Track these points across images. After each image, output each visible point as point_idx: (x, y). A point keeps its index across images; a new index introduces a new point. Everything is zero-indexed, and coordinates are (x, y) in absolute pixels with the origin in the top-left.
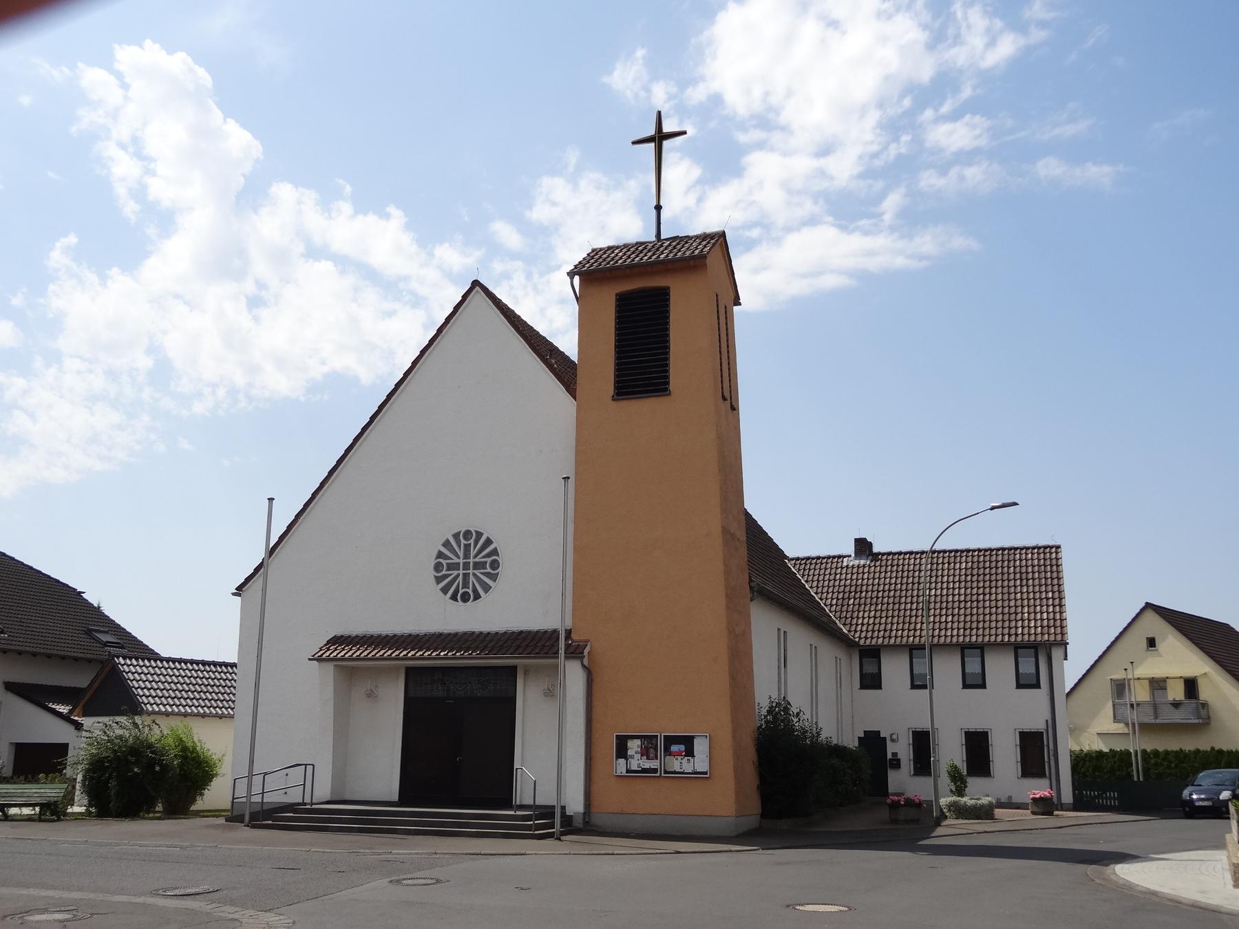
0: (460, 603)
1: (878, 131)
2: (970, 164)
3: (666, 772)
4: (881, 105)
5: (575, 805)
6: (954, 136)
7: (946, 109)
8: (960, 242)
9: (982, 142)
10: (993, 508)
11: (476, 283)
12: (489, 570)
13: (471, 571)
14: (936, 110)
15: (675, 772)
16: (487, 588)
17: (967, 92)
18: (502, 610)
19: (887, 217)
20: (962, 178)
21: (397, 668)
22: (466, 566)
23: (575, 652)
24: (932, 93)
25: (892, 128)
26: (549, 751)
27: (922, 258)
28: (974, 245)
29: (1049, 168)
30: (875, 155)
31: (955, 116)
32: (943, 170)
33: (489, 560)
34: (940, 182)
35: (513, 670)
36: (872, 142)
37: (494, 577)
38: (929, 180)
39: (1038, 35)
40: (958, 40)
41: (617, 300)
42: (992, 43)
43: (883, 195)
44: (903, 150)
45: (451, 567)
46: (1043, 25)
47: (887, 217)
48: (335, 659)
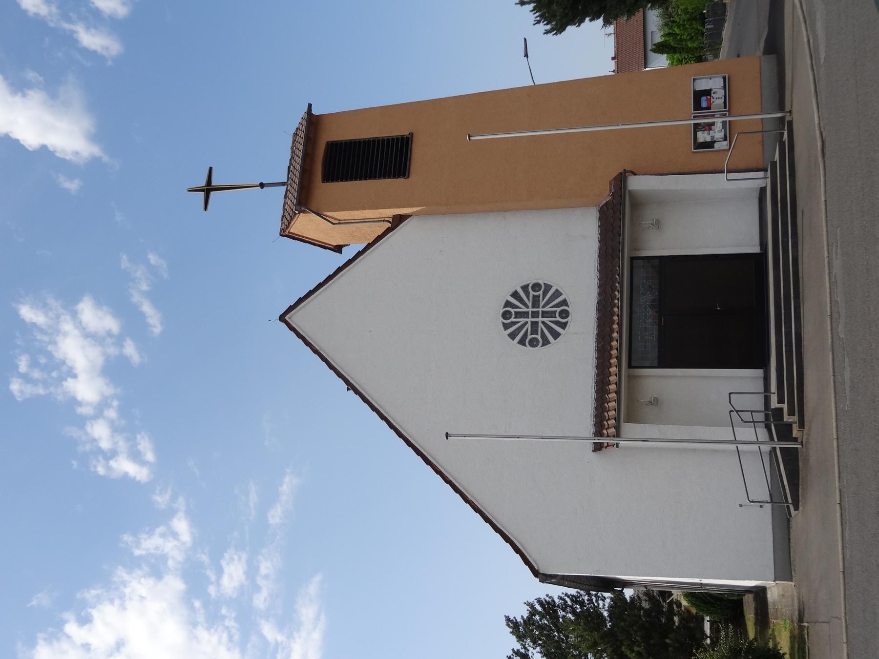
0: (569, 319)
1: (212, 630)
2: (258, 568)
3: (725, 107)
4: (194, 624)
5: (757, 180)
6: (233, 575)
7: (213, 578)
8: (313, 588)
9: (244, 556)
10: (526, 55)
11: (282, 318)
12: (541, 292)
13: (540, 310)
14: (212, 583)
15: (725, 103)
16: (558, 294)
17: (205, 558)
18: (577, 277)
19: (280, 638)
20: (266, 577)
21: (630, 377)
22: (535, 315)
23: (620, 181)
24: (196, 580)
25: (213, 619)
26: (710, 217)
27: (317, 619)
28: (318, 578)
29: (275, 516)
30: (230, 638)
31: (220, 572)
32: (257, 589)
33: (532, 293)
34: (265, 593)
35: (632, 259)
36: (220, 637)
37: (548, 287)
38: (260, 601)
39: (181, 502)
40: (164, 558)
41: (328, 181)
42: (175, 535)
43: (263, 638)
44: (233, 615)
45: (534, 330)
46: (174, 498)
47: (280, 638)
48: (618, 419)
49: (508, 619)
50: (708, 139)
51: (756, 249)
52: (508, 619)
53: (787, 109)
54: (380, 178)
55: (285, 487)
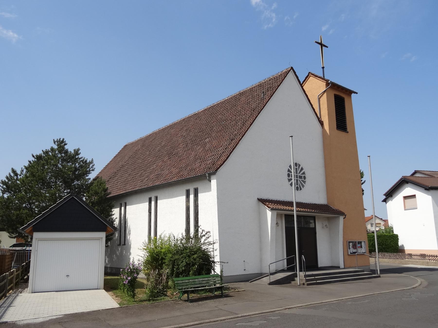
26: (330, 249)
35: (314, 218)
49: (79, 150)
50: (350, 247)
51: (320, 265)
52: (79, 150)
53: (381, 275)
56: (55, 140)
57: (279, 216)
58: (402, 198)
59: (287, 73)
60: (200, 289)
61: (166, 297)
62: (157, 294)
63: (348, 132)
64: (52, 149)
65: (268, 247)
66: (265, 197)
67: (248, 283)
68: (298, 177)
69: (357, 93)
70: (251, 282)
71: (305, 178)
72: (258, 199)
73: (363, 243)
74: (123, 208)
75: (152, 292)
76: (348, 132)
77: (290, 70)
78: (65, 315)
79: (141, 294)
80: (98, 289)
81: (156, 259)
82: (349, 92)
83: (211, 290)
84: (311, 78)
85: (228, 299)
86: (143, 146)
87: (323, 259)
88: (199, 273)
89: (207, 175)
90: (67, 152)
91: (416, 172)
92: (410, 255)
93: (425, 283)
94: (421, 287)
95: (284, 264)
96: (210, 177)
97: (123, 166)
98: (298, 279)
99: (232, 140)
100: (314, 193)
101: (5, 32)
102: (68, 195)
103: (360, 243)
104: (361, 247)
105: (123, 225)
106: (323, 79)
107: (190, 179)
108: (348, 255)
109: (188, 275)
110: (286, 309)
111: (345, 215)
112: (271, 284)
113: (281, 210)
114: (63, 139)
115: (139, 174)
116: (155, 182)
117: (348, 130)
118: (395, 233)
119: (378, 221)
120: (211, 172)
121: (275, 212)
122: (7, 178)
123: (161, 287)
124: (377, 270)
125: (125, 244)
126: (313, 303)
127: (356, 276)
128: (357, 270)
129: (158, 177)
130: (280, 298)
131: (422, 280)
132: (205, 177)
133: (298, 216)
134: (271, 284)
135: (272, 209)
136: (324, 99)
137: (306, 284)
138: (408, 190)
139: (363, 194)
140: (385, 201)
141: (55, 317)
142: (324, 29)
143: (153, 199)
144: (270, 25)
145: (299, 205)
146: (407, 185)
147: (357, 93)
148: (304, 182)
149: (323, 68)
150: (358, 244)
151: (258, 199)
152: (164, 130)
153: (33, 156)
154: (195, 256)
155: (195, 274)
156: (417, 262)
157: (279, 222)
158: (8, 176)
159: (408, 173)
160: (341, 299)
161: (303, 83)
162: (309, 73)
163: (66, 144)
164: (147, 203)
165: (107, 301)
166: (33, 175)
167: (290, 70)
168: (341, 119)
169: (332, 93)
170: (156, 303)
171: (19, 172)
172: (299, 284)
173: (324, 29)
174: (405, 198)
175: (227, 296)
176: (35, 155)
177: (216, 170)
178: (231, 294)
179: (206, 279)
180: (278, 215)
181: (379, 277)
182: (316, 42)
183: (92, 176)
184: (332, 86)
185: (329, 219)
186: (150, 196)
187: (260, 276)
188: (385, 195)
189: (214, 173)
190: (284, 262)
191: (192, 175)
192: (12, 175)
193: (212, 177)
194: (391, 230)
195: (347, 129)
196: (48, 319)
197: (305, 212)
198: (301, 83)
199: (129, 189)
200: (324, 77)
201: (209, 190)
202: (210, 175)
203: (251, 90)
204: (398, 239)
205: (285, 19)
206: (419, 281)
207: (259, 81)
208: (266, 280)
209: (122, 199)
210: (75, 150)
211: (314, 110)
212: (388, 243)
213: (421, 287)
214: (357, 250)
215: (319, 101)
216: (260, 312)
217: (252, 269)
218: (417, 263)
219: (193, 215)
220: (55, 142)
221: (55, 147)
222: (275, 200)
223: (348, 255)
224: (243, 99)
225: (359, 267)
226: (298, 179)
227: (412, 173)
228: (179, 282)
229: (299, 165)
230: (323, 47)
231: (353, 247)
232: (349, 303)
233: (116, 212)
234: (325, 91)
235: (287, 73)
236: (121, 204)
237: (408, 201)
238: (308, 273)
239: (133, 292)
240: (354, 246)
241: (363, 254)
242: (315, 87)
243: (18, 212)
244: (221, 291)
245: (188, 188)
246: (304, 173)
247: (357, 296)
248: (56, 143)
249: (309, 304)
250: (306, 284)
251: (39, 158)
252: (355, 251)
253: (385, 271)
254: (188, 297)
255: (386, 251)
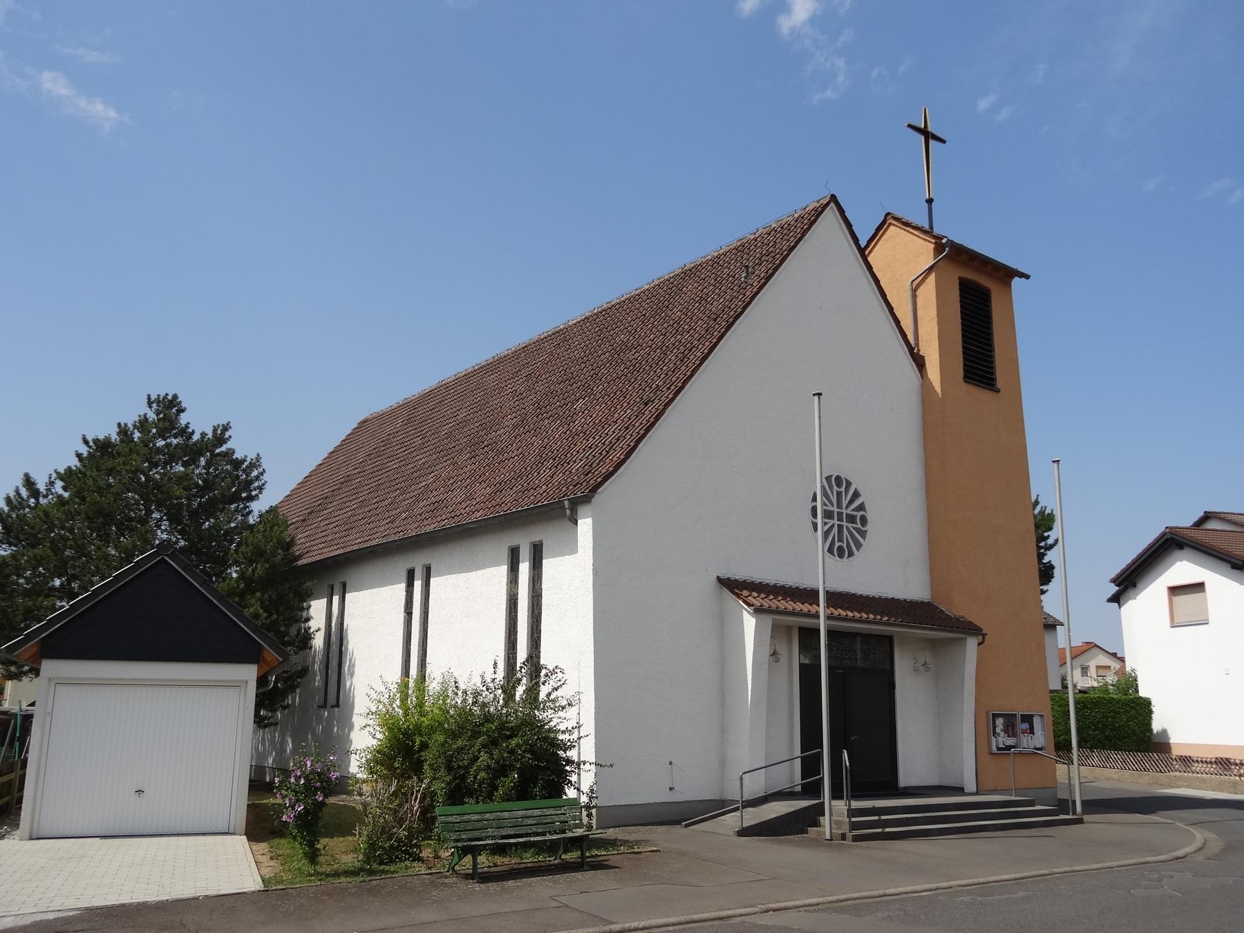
21: (789, 628)
26: (934, 734)
35: (889, 640)
41: (960, 284)
49: (226, 428)
50: (998, 730)
51: (903, 781)
52: (226, 428)
53: (1086, 818)
54: (964, 347)
55: (100, 107)
56: (153, 397)
57: (778, 631)
58: (1165, 593)
59: (819, 212)
60: (512, 841)
61: (415, 864)
62: (389, 852)
63: (998, 391)
64: (143, 424)
65: (746, 721)
66: (740, 574)
67: (678, 830)
68: (843, 517)
69: (1027, 277)
70: (687, 826)
71: (864, 521)
72: (720, 580)
73: (1036, 721)
74: (336, 599)
75: (372, 846)
76: (998, 391)
77: (828, 204)
78: (87, 909)
79: (343, 851)
80: (228, 833)
81: (403, 750)
82: (1006, 274)
83: (552, 848)
84: (893, 231)
85: (600, 874)
86: (409, 421)
87: (914, 765)
88: (522, 793)
89: (566, 503)
90: (185, 432)
91: (1207, 517)
92: (1186, 761)
93: (1216, 844)
94: (1200, 858)
95: (793, 775)
96: (574, 511)
97: (348, 479)
98: (825, 820)
99: (646, 404)
100: (891, 565)
101: (83, 103)
102: (169, 559)
103: (1028, 719)
104: (1032, 732)
105: (334, 648)
106: (929, 232)
107: (521, 519)
108: (987, 755)
109: (490, 797)
110: (767, 911)
111: (984, 635)
112: (744, 832)
113: (785, 612)
114: (175, 397)
115: (387, 502)
116: (426, 522)
117: (999, 384)
118: (1142, 693)
119: (1103, 660)
120: (579, 494)
121: (768, 620)
122: (8, 500)
123: (403, 833)
124: (1074, 802)
125: (337, 705)
126: (856, 895)
127: (1006, 818)
128: (1013, 798)
129: (436, 507)
130: (760, 877)
131: (1210, 836)
132: (560, 510)
133: (831, 633)
134: (744, 832)
135: (758, 611)
136: (929, 290)
137: (849, 836)
138: (1182, 569)
139: (1046, 573)
140: (1116, 599)
141: (51, 916)
142: (983, 104)
143: (418, 574)
144: (829, 93)
145: (836, 599)
146: (1178, 553)
147: (1027, 277)
148: (863, 534)
149: (930, 201)
150: (1023, 721)
151: (720, 580)
152: (468, 376)
153: (86, 442)
154: (514, 742)
155: (507, 798)
156: (1204, 781)
157: (782, 650)
158: (12, 494)
159: (1185, 519)
160: (945, 884)
161: (867, 246)
162: (888, 214)
163: (183, 411)
164: (403, 586)
165: (234, 866)
166: (79, 494)
167: (828, 204)
168: (980, 349)
169: (954, 274)
170: (375, 881)
171: (42, 487)
172: (828, 836)
173: (983, 104)
174: (1174, 590)
175: (599, 866)
176: (90, 438)
177: (594, 490)
178: (613, 860)
179: (537, 812)
180: (776, 628)
181: (1080, 821)
182: (910, 126)
183: (259, 506)
184: (953, 255)
185: (934, 644)
186: (409, 566)
187: (717, 807)
188: (1113, 581)
189: (586, 499)
190: (792, 769)
191: (526, 503)
192: (24, 493)
193: (582, 510)
194: (1130, 683)
195: (995, 380)
196: (28, 921)
197: (860, 621)
198: (863, 244)
199: (355, 542)
200: (931, 227)
201: (572, 548)
202: (576, 503)
203: (716, 261)
204: (1151, 712)
205: (875, 74)
206: (1199, 836)
207: (739, 235)
208: (731, 821)
209: (334, 573)
210: (215, 430)
211: (897, 322)
212: (1120, 722)
213: (1200, 858)
214: (1019, 740)
215: (914, 297)
216: (682, 919)
217: (693, 788)
218: (1202, 785)
219: (525, 620)
220: (150, 404)
221: (152, 416)
222: (773, 582)
223: (991, 754)
224: (691, 286)
225: (1018, 791)
226: (844, 523)
227: (1195, 518)
228: (450, 819)
229: (849, 484)
230: (931, 142)
231: (1006, 730)
232: (966, 899)
233: (317, 609)
234: (931, 269)
235: (819, 212)
236: (332, 587)
237: (1180, 599)
238: (856, 804)
239: (311, 844)
240: (1010, 729)
241: (1036, 752)
242: (904, 258)
243: (31, 603)
244: (577, 852)
245: (514, 543)
246: (861, 507)
247: (997, 878)
248: (154, 405)
249: (843, 897)
250: (849, 836)
251: (103, 446)
252: (1011, 741)
253: (1096, 805)
254: (475, 863)
255: (1116, 748)
